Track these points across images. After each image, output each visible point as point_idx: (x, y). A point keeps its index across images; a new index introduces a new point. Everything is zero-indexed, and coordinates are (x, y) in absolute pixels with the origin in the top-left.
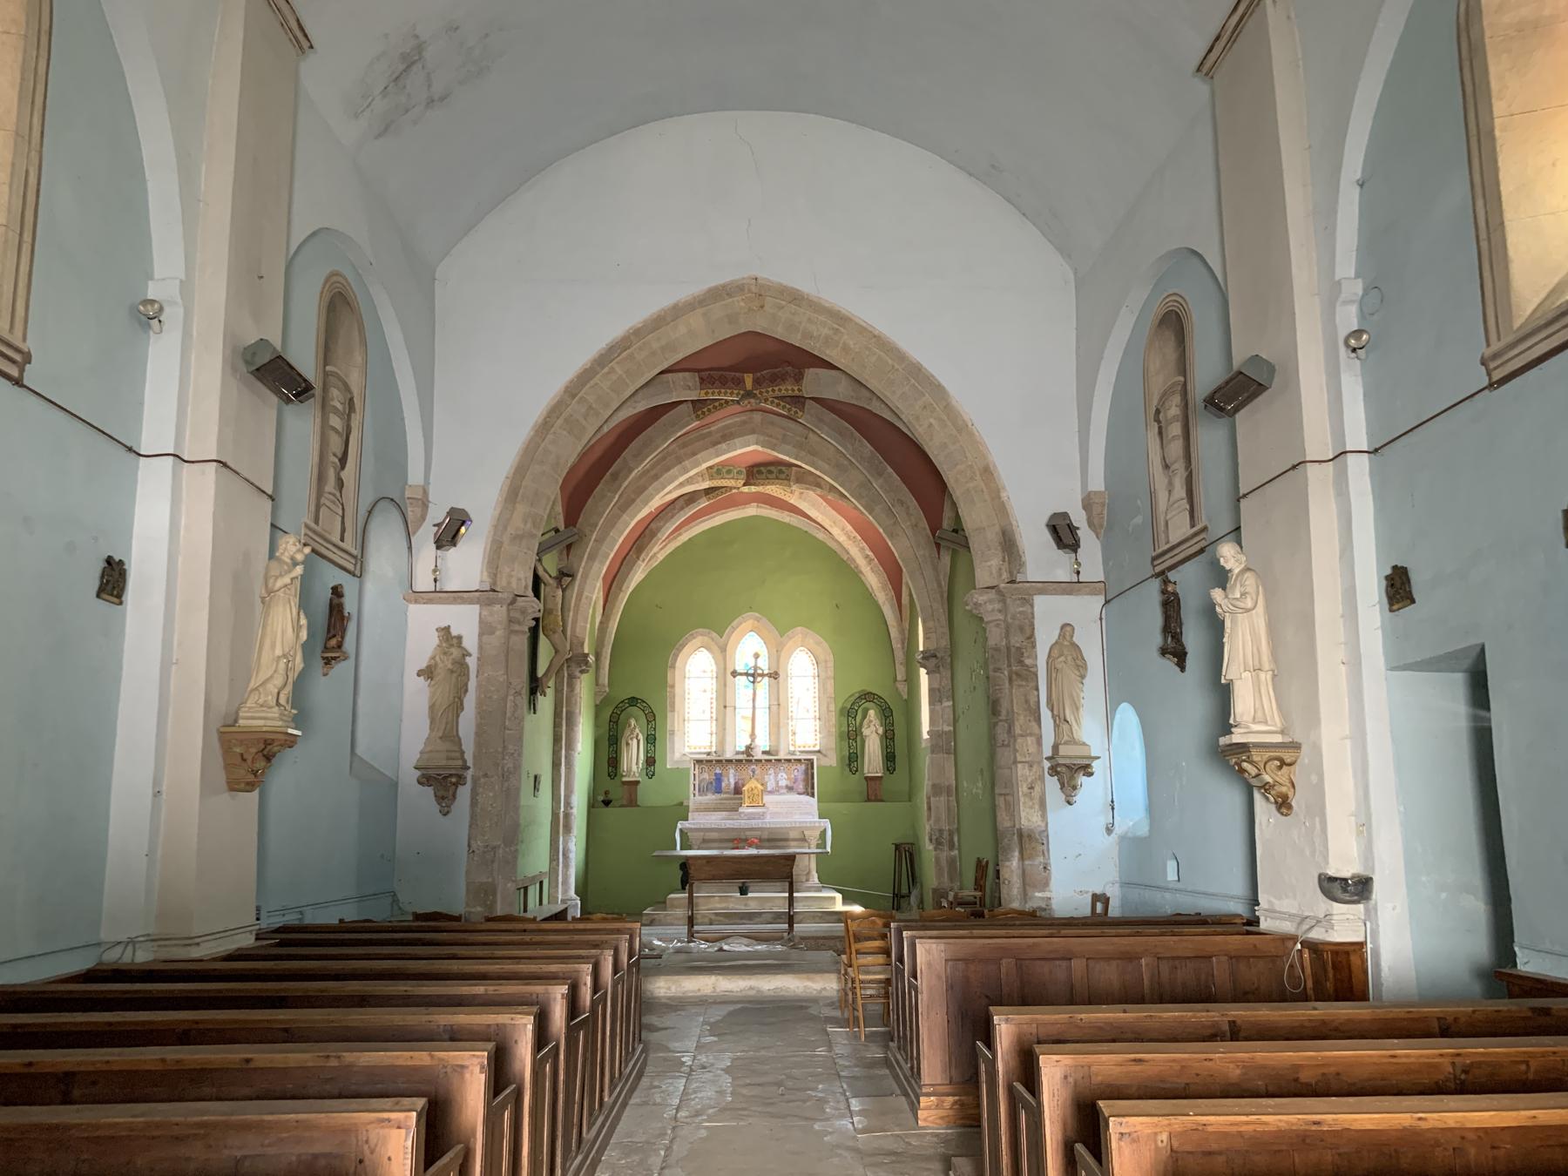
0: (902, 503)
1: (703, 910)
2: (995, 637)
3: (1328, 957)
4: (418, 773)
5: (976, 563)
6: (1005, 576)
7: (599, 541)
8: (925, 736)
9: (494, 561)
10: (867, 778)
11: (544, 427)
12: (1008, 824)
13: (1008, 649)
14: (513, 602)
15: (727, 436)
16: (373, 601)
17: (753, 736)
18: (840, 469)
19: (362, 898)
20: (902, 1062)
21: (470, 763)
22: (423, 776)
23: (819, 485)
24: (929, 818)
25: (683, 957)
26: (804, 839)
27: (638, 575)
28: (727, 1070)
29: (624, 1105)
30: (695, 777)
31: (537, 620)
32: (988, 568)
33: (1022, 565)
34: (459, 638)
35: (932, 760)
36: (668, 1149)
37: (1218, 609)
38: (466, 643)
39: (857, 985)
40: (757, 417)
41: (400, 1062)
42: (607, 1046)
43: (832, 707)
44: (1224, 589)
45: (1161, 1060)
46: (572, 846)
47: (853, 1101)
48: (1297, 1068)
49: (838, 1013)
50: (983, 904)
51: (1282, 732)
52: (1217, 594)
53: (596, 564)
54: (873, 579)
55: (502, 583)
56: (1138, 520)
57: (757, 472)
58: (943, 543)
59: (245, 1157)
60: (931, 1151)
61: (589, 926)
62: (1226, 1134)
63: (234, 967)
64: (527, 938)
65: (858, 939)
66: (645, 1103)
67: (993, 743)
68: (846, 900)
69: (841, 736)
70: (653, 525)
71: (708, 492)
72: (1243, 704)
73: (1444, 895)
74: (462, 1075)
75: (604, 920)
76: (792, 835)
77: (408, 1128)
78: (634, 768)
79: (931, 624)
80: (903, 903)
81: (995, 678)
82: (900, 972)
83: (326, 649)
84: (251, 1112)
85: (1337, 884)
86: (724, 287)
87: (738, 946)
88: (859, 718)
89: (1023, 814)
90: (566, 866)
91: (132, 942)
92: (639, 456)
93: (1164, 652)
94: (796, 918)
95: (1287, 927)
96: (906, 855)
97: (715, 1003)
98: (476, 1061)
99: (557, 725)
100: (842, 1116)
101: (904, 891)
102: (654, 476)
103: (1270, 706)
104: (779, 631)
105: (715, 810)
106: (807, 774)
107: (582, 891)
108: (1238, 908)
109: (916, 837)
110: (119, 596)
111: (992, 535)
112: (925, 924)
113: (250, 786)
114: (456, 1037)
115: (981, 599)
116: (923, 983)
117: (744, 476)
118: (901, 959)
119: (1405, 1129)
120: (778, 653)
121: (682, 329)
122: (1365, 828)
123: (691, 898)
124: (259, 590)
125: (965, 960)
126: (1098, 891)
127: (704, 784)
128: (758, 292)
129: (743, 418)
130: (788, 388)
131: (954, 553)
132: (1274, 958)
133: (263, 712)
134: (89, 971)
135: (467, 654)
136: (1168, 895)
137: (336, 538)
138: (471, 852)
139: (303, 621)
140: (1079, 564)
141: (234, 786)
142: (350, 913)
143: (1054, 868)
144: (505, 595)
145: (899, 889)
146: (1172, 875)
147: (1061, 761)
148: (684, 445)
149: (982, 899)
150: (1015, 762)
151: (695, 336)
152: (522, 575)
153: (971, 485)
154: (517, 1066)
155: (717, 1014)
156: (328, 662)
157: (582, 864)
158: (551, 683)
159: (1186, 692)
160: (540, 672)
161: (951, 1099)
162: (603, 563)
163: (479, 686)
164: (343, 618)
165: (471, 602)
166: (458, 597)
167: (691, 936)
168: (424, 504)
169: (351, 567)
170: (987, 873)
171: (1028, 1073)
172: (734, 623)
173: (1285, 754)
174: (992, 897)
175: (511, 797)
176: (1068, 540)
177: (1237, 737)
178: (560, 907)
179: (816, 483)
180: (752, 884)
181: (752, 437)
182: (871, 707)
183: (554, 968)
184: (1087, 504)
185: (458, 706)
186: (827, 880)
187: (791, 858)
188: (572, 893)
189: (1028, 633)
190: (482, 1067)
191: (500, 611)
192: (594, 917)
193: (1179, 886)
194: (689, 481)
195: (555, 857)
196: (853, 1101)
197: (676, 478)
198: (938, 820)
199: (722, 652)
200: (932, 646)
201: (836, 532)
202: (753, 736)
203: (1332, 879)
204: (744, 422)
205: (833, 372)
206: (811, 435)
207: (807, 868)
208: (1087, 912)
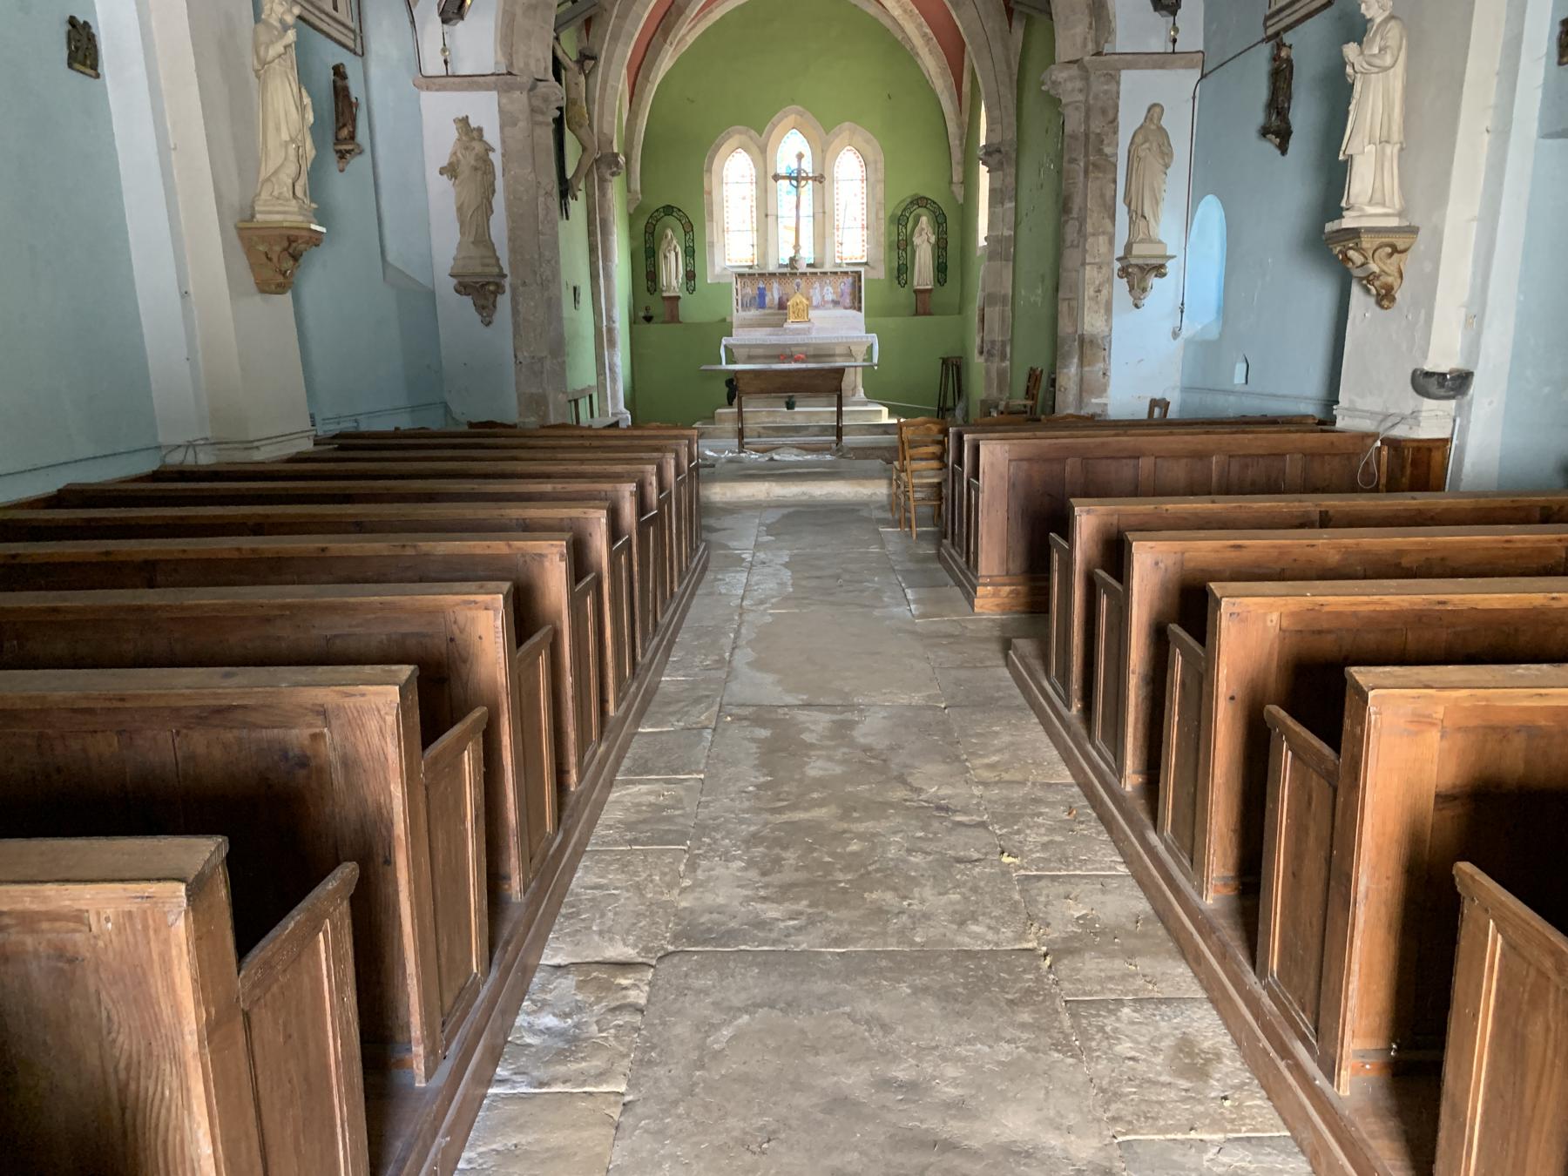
1: (751, 424)
2: (1074, 122)
3: (1409, 454)
4: (454, 281)
6: (1091, 47)
7: (623, 16)
8: (982, 242)
10: (916, 292)
12: (1070, 330)
13: (1087, 136)
14: (532, 88)
16: (380, 82)
17: (797, 247)
19: (413, 409)
20: (957, 557)
21: (506, 271)
22: (460, 283)
25: (734, 466)
26: (850, 355)
27: (666, 62)
28: (786, 565)
29: (692, 595)
31: (560, 109)
33: (1111, 32)
34: (480, 130)
36: (738, 632)
37: (1349, 70)
38: (487, 137)
41: (478, 551)
42: (669, 548)
43: (882, 214)
44: (1360, 43)
45: (1259, 545)
47: (908, 591)
48: (1401, 553)
49: (889, 515)
51: (1400, 215)
52: (1351, 50)
54: (931, 62)
55: (519, 64)
58: (1018, 8)
59: (336, 636)
60: (987, 634)
62: (1341, 613)
63: (296, 469)
65: (914, 445)
66: (711, 594)
68: (891, 414)
72: (1360, 184)
73: (1546, 390)
74: (541, 563)
75: (659, 428)
76: (838, 351)
77: (496, 610)
78: (674, 283)
82: (957, 475)
83: (338, 141)
84: (330, 595)
85: (1434, 380)
89: (1087, 319)
90: (614, 380)
91: (191, 445)
93: (1265, 132)
95: (1367, 425)
96: (954, 368)
98: (555, 550)
99: (591, 233)
100: (898, 605)
103: (1391, 182)
105: (760, 325)
106: (854, 283)
107: (631, 404)
108: (1310, 408)
110: (94, 66)
113: (281, 289)
114: (529, 528)
116: (985, 481)
118: (959, 460)
119: (1535, 608)
120: (823, 154)
122: (1475, 320)
123: (740, 412)
124: (250, 61)
125: (1029, 460)
126: (1158, 397)
127: (747, 299)
132: (1349, 456)
133: (282, 207)
134: (155, 473)
135: (489, 149)
136: (1232, 399)
137: (329, 8)
138: (518, 363)
139: (307, 100)
140: (1176, 30)
141: (265, 288)
142: (405, 422)
145: (944, 402)
146: (1239, 378)
147: (1133, 261)
150: (1084, 264)
152: (540, 55)
154: (593, 556)
155: (772, 517)
156: (342, 155)
157: (628, 379)
159: (1288, 181)
160: (569, 174)
161: (1007, 589)
162: (627, 45)
163: (507, 186)
164: (351, 104)
166: (472, 82)
167: (742, 447)
169: (350, 44)
170: (1041, 385)
171: (1115, 554)
172: (775, 119)
173: (1398, 241)
175: (552, 306)
177: (1348, 222)
178: (611, 420)
182: (922, 214)
183: (619, 468)
185: (488, 210)
186: (873, 395)
187: (840, 372)
189: (1111, 116)
190: (562, 555)
191: (520, 99)
193: (1247, 388)
195: (601, 371)
196: (908, 591)
199: (762, 154)
200: (997, 139)
202: (797, 247)
203: (1428, 374)
207: (854, 382)
208: (1145, 416)
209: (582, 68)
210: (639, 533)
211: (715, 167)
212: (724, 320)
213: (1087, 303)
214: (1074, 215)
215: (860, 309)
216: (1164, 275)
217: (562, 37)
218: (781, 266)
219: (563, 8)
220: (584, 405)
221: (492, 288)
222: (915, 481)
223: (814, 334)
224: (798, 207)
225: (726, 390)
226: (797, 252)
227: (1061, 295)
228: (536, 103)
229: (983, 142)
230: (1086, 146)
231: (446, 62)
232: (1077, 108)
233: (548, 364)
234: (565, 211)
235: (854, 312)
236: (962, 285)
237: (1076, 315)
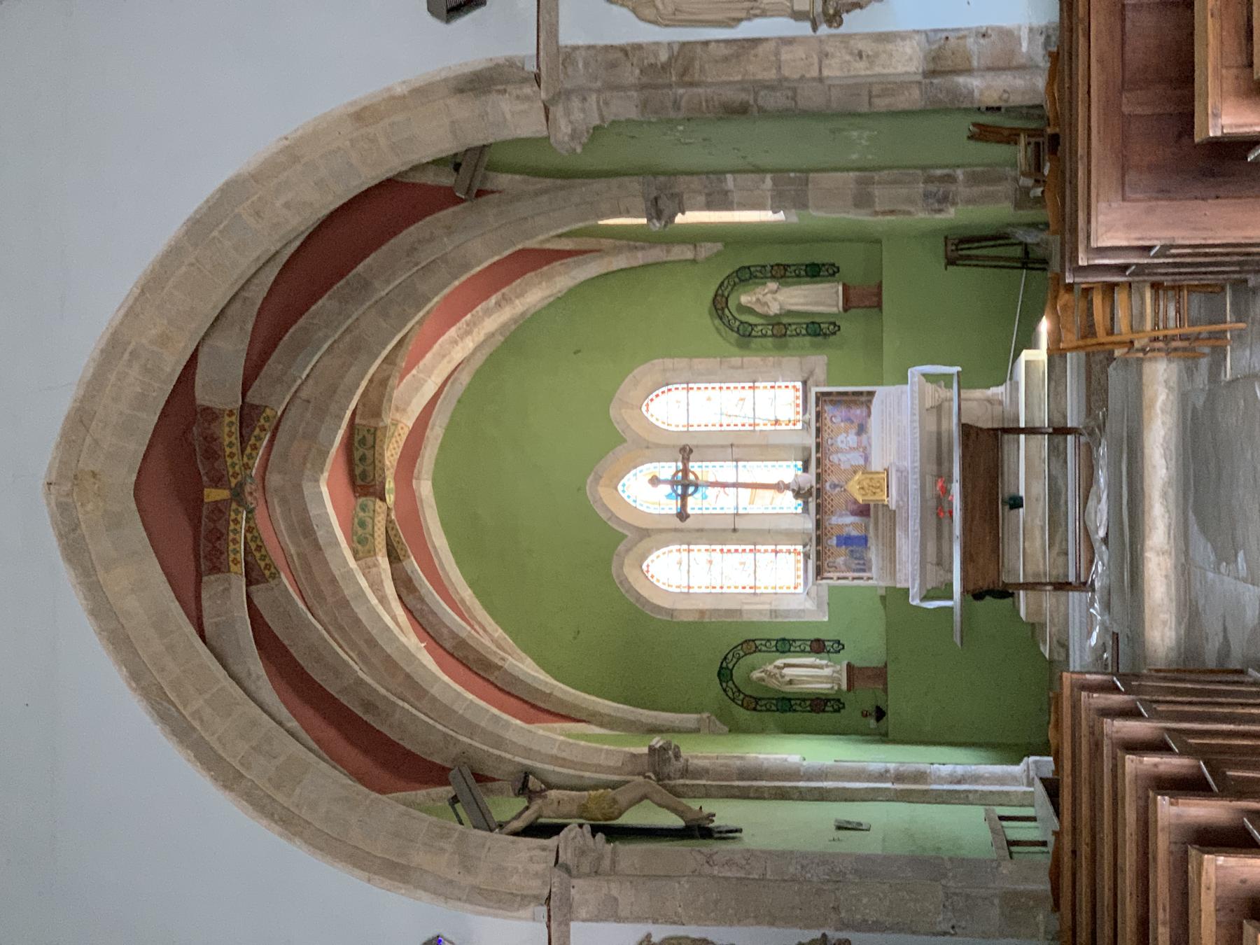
0: (412, 250)
2: (625, 108)
5: (507, 134)
6: (528, 90)
7: (472, 729)
8: (780, 216)
10: (845, 310)
11: (289, 822)
12: (916, 93)
15: (306, 529)
17: (780, 487)
18: (359, 349)
21: (816, 934)
23: (384, 383)
24: (909, 213)
25: (1115, 600)
26: (939, 409)
27: (526, 667)
30: (842, 578)
32: (515, 117)
33: (511, 63)
35: (818, 208)
39: (1160, 334)
40: (274, 479)
43: (736, 361)
46: (946, 770)
49: (1204, 363)
50: (1039, 132)
53: (509, 735)
54: (534, 294)
55: (536, 887)
57: (362, 481)
58: (477, 186)
61: (1067, 751)
64: (1085, 850)
65: (1089, 330)
67: (791, 114)
68: (1031, 343)
70: (448, 645)
75: (1058, 725)
76: (933, 428)
80: (1038, 253)
86: (61, 536)
87: (1100, 516)
88: (752, 319)
89: (901, 69)
90: (976, 779)
92: (339, 669)
96: (963, 248)
97: (1186, 553)
99: (759, 795)
101: (1018, 252)
102: (370, 645)
104: (616, 444)
106: (835, 404)
107: (1014, 753)
109: (934, 233)
111: (463, 109)
112: (1068, 226)
115: (564, 128)
117: (368, 501)
118: (1122, 268)
120: (653, 445)
121: (131, 603)
123: (1027, 586)
128: (70, 483)
129: (275, 502)
130: (228, 432)
131: (494, 168)
143: (983, 22)
145: (1021, 261)
148: (319, 595)
149: (1031, 133)
150: (820, 80)
151: (143, 583)
153: (383, 141)
155: (1203, 550)
158: (694, 805)
160: (676, 822)
162: (507, 725)
163: (698, 921)
167: (1084, 586)
170: (991, 127)
172: (603, 515)
174: (1028, 117)
175: (868, 869)
178: (1039, 789)
179: (381, 385)
180: (1006, 491)
181: (307, 488)
183: (1130, 814)
186: (1000, 371)
187: (967, 431)
188: (1017, 770)
189: (620, 55)
191: (583, 891)
192: (1053, 742)
194: (376, 586)
195: (960, 799)
197: (372, 610)
198: (910, 200)
199: (649, 535)
200: (640, 203)
201: (458, 354)
202: (780, 487)
204: (284, 501)
205: (202, 359)
206: (304, 394)
207: (983, 403)
209: (539, 794)
210: (1240, 795)
212: (883, 598)
213: (878, 70)
215: (871, 394)
218: (806, 509)
220: (1017, 831)
222: (1149, 325)
223: (907, 464)
224: (724, 485)
225: (988, 600)
226: (787, 487)
227: (865, 108)
228: (586, 868)
229: (644, 221)
230: (656, 87)
232: (606, 103)
234: (729, 834)
235: (876, 401)
237: (894, 86)
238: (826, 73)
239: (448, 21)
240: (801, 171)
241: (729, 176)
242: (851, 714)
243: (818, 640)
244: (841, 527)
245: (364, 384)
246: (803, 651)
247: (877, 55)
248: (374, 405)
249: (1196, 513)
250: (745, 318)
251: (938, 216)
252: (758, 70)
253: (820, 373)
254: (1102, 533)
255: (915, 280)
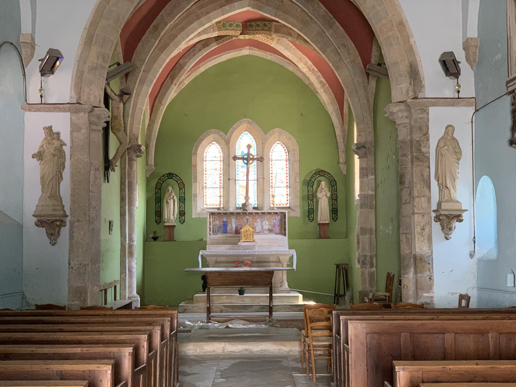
0: (344, 46)
2: (403, 134)
4: (35, 219)
6: (411, 94)
8: (357, 198)
9: (79, 83)
10: (319, 224)
12: (407, 252)
13: (411, 142)
14: (92, 111)
17: (247, 197)
18: (304, 24)
21: (68, 213)
23: (290, 34)
25: (204, 331)
27: (172, 94)
30: (210, 223)
31: (107, 122)
32: (400, 89)
33: (422, 87)
34: (58, 134)
38: (62, 138)
43: (298, 180)
49: (299, 365)
54: (325, 97)
56: (499, 56)
57: (249, 25)
65: (312, 321)
69: (303, 198)
71: (218, 38)
75: (155, 309)
78: (172, 217)
79: (362, 126)
81: (401, 159)
82: (338, 341)
90: (131, 276)
92: (171, 14)
94: (274, 309)
96: (343, 271)
97: (224, 359)
99: (122, 190)
105: (224, 243)
106: (281, 220)
107: (141, 291)
111: (404, 67)
112: (354, 312)
117: (241, 28)
120: (263, 145)
123: (209, 297)
125: (379, 333)
126: (463, 293)
127: (216, 228)
135: (63, 144)
136: (507, 296)
138: (71, 268)
140: (459, 86)
144: (87, 106)
145: (338, 293)
146: (510, 283)
150: (413, 213)
155: (225, 365)
160: (111, 157)
162: (149, 86)
163: (72, 165)
165: (64, 111)
166: (57, 107)
168: (33, 46)
170: (393, 282)
172: (234, 126)
175: (95, 234)
176: (453, 70)
178: (127, 302)
179: (289, 33)
184: (466, 47)
185: (59, 177)
186: (294, 286)
187: (271, 273)
189: (425, 131)
191: (83, 118)
194: (205, 32)
195: (123, 271)
197: (196, 29)
199: (227, 145)
200: (363, 140)
201: (301, 65)
202: (247, 197)
207: (281, 279)
209: (121, 100)
211: (199, 152)
212: (202, 240)
213: (417, 236)
214: (406, 185)
215: (285, 235)
216: (461, 221)
217: (111, 83)
218: (238, 208)
219: (112, 68)
220: (110, 293)
221: (58, 223)
222: (314, 343)
223: (257, 249)
224: (247, 175)
227: (401, 231)
229: (355, 142)
230: (411, 147)
231: (41, 96)
232: (405, 127)
233: (89, 268)
234: (107, 177)
235: (281, 236)
236: (347, 223)
237: (410, 243)
238: (416, 215)
239: (440, 61)
240: (376, 206)
241: (374, 177)
242: (155, 227)
243: (185, 213)
244: (231, 223)
245: (290, 26)
246: (180, 207)
247: (423, 236)
248: (280, 30)
249: (240, 363)
250: (315, 183)
251: (356, 261)
252: (418, 189)
253: (293, 214)
254: (230, 326)
255: (330, 251)
